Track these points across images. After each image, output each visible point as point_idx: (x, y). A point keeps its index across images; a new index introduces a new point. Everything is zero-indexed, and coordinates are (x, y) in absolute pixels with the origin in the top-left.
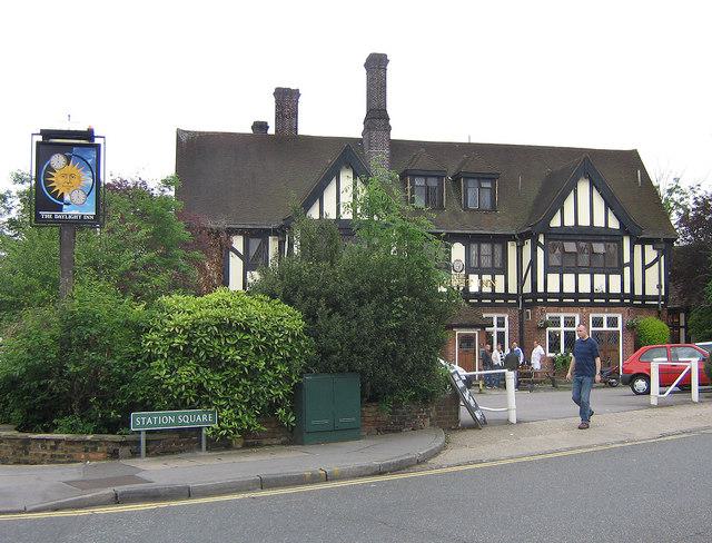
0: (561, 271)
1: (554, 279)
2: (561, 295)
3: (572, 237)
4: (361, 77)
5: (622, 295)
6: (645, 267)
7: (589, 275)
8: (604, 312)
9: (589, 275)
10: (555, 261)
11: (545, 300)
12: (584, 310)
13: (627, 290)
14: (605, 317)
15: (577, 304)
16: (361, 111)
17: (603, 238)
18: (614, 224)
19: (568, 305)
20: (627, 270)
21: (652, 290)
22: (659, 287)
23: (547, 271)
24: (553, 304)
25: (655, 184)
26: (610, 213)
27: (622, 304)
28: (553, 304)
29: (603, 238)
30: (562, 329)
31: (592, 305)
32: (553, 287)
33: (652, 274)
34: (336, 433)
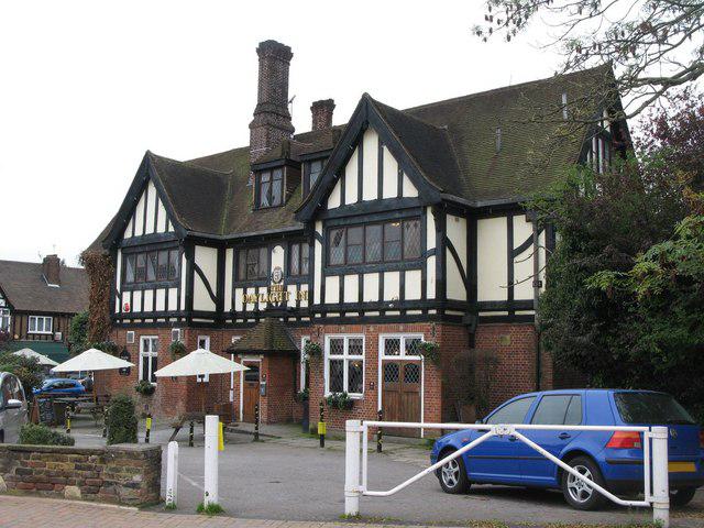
0: (342, 273)
1: (333, 283)
2: (342, 307)
3: (356, 220)
4: (251, 68)
5: (423, 303)
6: (513, 253)
7: (377, 275)
8: (398, 331)
9: (377, 275)
10: (337, 256)
11: (324, 314)
12: (371, 329)
13: (431, 294)
14: (402, 338)
15: (362, 320)
16: (250, 99)
17: (397, 215)
18: (410, 191)
19: (351, 321)
20: (432, 262)
21: (525, 292)
22: (537, 284)
23: (324, 276)
24: (332, 321)
25: (290, 98)
26: (406, 178)
27: (424, 318)
28: (332, 321)
29: (397, 215)
30: (345, 356)
31: (383, 320)
32: (332, 297)
33: (524, 267)
34: (597, 387)
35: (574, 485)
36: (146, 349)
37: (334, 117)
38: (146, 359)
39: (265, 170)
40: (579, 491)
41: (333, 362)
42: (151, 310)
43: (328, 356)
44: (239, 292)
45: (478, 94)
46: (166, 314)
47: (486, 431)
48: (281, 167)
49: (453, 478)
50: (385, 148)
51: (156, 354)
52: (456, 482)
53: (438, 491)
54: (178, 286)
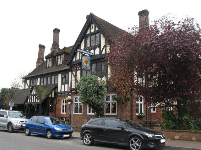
4: (52, 34)
35: (86, 139)
36: (63, 103)
37: (60, 44)
38: (63, 106)
39: (59, 55)
40: (135, 146)
41: (75, 104)
42: (63, 91)
43: (74, 102)
44: (63, 86)
45: (103, 20)
46: (65, 92)
47: (89, 123)
48: (62, 54)
49: (89, 140)
50: (102, 34)
51: (137, 102)
52: (90, 142)
53: (83, 144)
54: (68, 84)
